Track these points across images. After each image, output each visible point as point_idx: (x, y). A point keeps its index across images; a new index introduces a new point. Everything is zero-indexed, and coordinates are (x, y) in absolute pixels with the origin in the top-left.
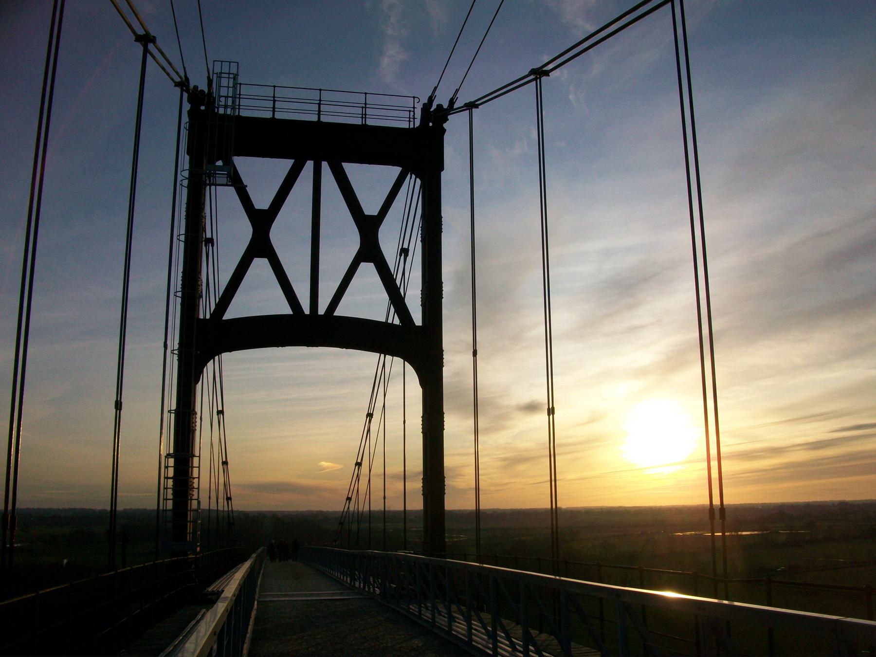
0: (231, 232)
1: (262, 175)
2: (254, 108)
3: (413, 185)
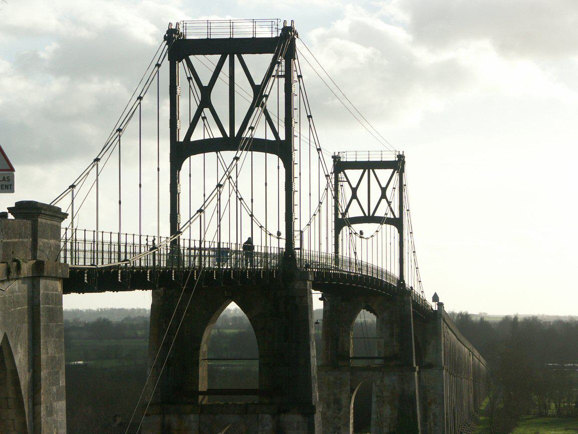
0: (346, 192)
1: (353, 175)
2: (350, 158)
3: (396, 176)
